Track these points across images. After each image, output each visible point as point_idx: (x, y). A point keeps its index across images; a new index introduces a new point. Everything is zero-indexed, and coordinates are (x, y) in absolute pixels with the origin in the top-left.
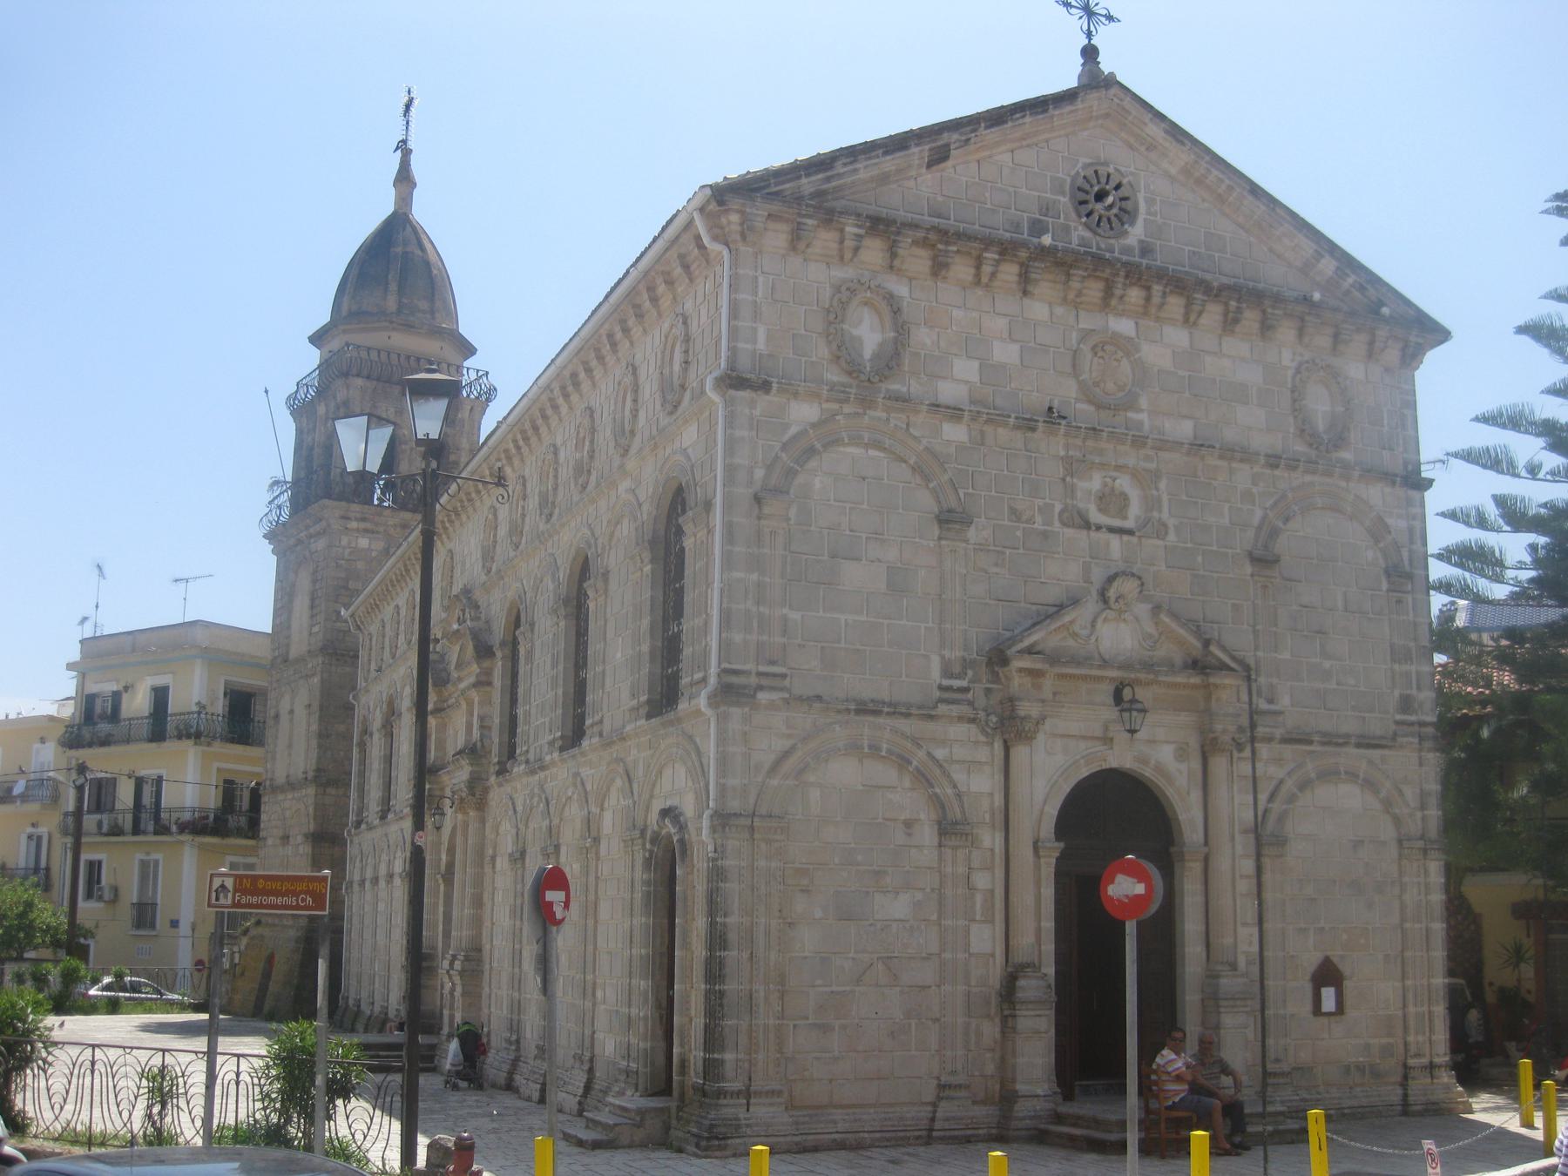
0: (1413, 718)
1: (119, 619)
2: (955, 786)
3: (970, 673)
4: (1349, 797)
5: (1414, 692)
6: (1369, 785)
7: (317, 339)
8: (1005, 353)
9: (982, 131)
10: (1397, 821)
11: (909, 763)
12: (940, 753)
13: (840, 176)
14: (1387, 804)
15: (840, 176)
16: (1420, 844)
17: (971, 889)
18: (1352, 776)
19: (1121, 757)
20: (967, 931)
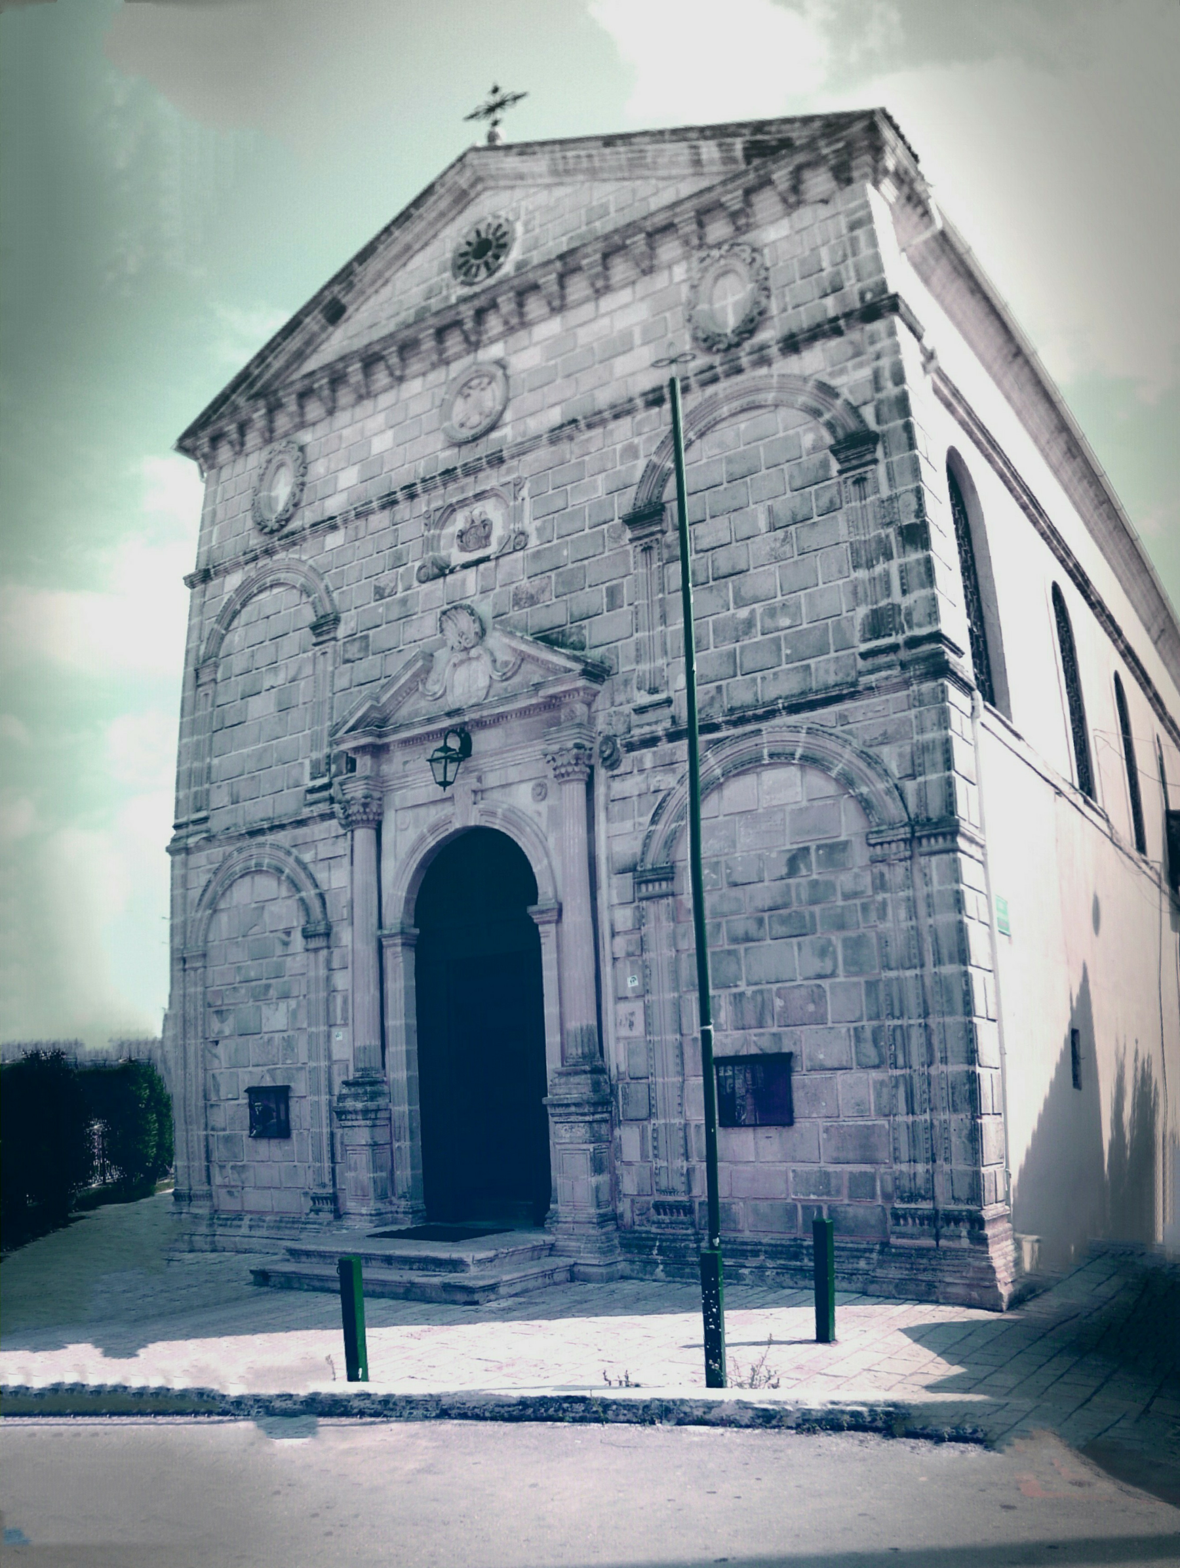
0: (899, 639)
1: (704, 1382)
2: (317, 886)
3: (333, 768)
4: (784, 787)
5: (897, 597)
6: (810, 761)
7: (896, 296)
8: (381, 443)
9: (397, 233)
10: (866, 805)
11: (282, 872)
12: (307, 857)
13: (259, 376)
14: (847, 782)
15: (259, 376)
16: (904, 833)
17: (332, 991)
18: (781, 758)
19: (465, 815)
20: (329, 1036)
